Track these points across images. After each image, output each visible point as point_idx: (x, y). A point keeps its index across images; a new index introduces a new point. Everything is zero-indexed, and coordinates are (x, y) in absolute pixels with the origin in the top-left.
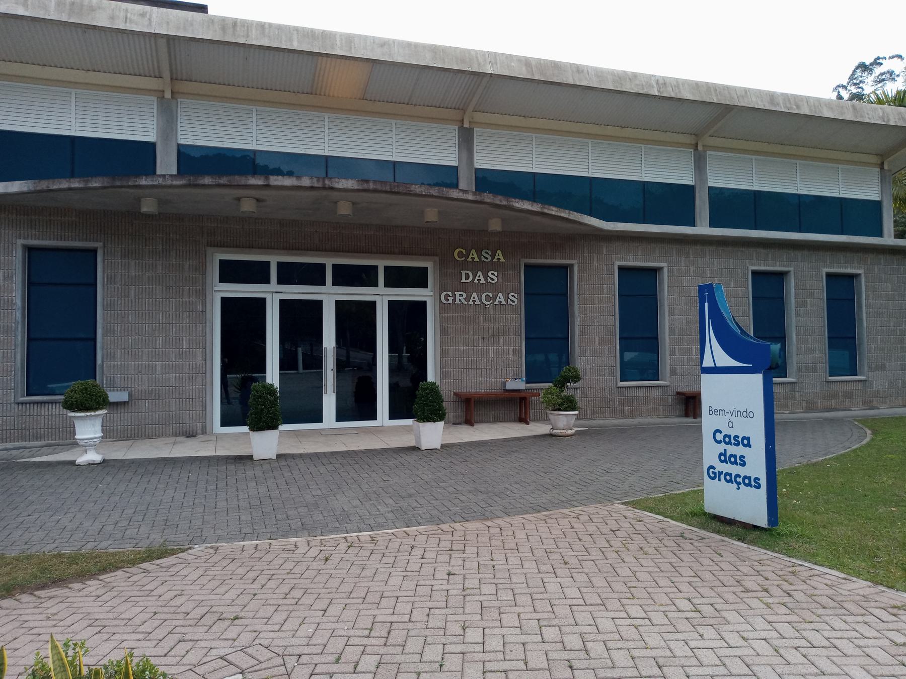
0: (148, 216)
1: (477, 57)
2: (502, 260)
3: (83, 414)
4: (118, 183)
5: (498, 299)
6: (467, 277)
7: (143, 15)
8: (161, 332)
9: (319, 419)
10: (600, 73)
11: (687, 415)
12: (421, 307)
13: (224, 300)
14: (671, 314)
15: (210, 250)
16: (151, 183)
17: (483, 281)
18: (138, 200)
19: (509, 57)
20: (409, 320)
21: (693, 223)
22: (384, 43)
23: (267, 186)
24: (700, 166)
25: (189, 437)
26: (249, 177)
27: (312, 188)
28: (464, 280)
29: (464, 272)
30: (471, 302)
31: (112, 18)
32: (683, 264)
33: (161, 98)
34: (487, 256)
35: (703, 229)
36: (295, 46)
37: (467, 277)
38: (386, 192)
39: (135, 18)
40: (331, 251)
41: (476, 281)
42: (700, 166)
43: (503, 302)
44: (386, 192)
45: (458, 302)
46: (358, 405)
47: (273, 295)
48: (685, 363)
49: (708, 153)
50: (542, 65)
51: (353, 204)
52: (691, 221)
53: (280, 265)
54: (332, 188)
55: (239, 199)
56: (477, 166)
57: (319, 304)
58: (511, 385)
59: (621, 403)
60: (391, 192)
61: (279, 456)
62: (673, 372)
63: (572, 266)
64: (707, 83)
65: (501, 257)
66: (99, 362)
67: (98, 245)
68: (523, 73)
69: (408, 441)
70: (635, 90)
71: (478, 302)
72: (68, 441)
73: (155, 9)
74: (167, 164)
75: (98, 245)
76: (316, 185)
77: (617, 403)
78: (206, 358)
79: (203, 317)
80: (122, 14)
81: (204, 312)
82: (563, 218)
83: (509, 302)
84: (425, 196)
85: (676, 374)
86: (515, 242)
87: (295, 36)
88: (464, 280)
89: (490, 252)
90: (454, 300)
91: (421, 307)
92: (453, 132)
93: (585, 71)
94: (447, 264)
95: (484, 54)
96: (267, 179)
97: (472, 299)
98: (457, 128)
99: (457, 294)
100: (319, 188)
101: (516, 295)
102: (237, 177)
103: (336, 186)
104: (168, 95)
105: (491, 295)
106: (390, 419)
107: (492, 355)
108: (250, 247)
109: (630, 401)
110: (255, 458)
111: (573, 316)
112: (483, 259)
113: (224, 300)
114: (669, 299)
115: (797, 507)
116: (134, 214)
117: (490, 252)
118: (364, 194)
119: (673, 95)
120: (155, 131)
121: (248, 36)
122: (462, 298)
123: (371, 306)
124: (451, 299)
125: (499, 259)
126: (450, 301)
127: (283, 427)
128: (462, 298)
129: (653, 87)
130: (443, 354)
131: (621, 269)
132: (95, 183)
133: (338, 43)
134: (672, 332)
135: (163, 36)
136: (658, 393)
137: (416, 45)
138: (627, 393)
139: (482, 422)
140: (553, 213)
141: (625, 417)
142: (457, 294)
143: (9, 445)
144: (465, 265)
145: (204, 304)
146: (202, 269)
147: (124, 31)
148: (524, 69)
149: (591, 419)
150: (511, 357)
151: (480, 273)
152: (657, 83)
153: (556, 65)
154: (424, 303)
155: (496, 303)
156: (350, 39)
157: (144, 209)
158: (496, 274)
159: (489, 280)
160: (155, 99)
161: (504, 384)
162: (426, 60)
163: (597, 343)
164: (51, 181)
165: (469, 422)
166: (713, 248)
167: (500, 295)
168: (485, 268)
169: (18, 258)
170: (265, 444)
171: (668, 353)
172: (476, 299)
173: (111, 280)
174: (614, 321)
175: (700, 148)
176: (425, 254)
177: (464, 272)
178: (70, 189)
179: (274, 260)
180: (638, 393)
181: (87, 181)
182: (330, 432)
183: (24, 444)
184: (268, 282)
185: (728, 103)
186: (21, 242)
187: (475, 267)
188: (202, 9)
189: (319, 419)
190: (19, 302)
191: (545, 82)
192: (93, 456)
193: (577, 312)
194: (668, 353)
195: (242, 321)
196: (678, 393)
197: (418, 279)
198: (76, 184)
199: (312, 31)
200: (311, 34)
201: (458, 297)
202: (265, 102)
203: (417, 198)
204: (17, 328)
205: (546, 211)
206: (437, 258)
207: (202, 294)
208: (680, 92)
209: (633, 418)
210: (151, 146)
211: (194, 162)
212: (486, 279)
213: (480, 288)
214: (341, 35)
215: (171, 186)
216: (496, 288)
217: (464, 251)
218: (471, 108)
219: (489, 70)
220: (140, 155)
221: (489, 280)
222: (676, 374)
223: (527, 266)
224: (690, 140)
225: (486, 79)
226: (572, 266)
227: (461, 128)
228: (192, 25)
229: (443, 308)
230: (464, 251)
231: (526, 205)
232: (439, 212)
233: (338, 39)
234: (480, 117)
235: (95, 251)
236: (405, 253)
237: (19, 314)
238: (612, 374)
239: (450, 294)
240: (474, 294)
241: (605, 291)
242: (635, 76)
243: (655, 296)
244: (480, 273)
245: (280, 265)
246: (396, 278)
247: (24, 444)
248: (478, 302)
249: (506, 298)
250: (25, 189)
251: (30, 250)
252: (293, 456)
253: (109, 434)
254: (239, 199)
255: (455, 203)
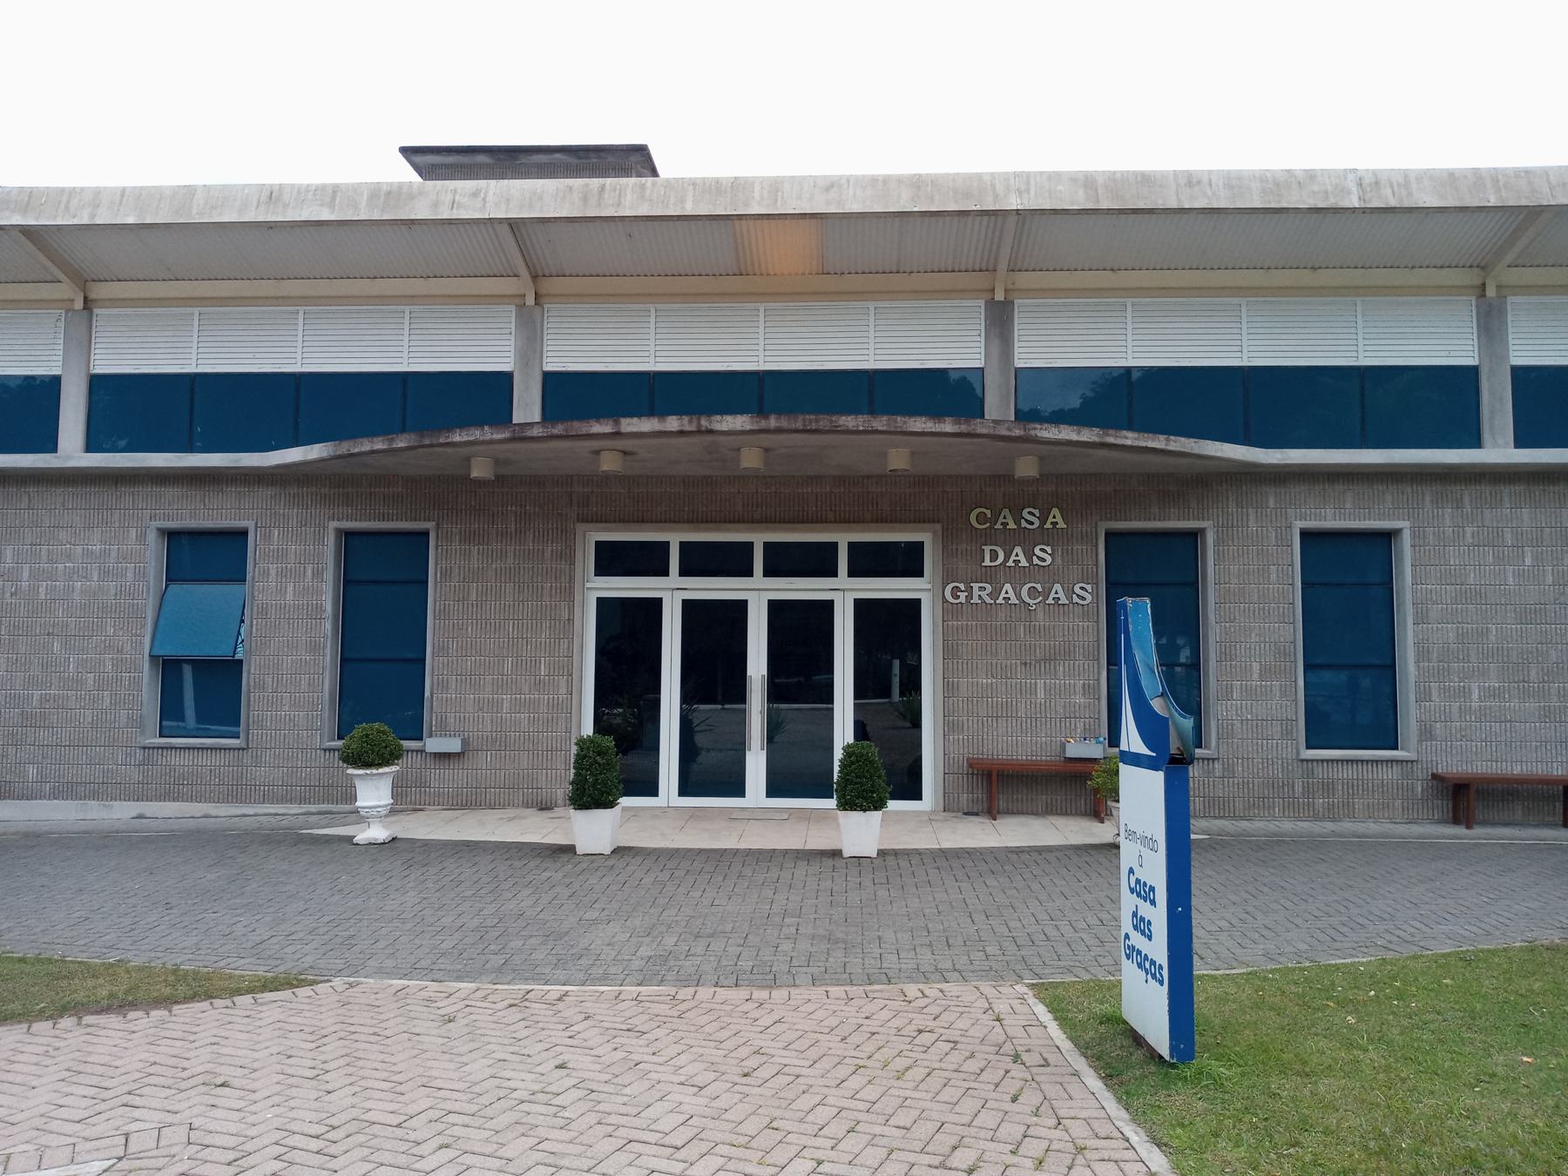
0: (480, 483)
1: (993, 185)
2: (1061, 525)
3: (361, 772)
4: (427, 442)
5: (1052, 595)
6: (994, 556)
7: (475, 195)
8: (514, 656)
9: (740, 792)
10: (1234, 180)
11: (1456, 821)
12: (910, 610)
13: (601, 602)
14: (1421, 618)
15: (580, 527)
16: (466, 438)
17: (1024, 563)
18: (467, 460)
19: (1055, 177)
20: (891, 632)
21: (1477, 443)
22: (831, 185)
23: (617, 434)
24: (1491, 324)
25: (542, 809)
26: (593, 422)
27: (681, 433)
28: (987, 562)
29: (987, 549)
30: (1000, 601)
31: (436, 205)
32: (1448, 522)
33: (521, 306)
34: (1031, 517)
35: (1499, 450)
36: (689, 209)
37: (994, 556)
38: (796, 431)
39: (465, 200)
40: (760, 522)
41: (1010, 563)
42: (1491, 324)
43: (1064, 600)
44: (796, 431)
45: (975, 600)
46: (711, 774)
47: (673, 593)
48: (1456, 716)
49: (1510, 299)
50: (1116, 181)
51: (766, 450)
52: (1474, 439)
53: (684, 546)
54: (711, 432)
55: (597, 452)
56: (1019, 364)
57: (742, 606)
58: (1076, 750)
59: (1308, 790)
60: (805, 431)
61: (618, 851)
62: (1426, 733)
63: (1202, 531)
64: (1476, 171)
65: (1059, 519)
66: (427, 694)
67: (430, 525)
68: (1080, 201)
69: (818, 840)
70: (1309, 203)
71: (1014, 600)
72: (347, 807)
73: (493, 182)
74: (527, 407)
75: (430, 525)
76: (687, 428)
77: (1298, 789)
78: (573, 691)
79: (567, 627)
80: (449, 198)
81: (570, 620)
82: (1154, 450)
83: (1075, 599)
84: (865, 432)
85: (1432, 738)
86: (1075, 491)
87: (690, 194)
88: (987, 562)
89: (1037, 512)
90: (969, 597)
91: (910, 610)
92: (976, 308)
93: (1205, 180)
94: (954, 531)
95: (1006, 177)
96: (617, 423)
97: (1003, 594)
98: (982, 303)
99: (975, 586)
100: (691, 433)
101: (1089, 588)
102: (576, 424)
103: (717, 427)
104: (530, 301)
105: (1039, 587)
106: (920, 798)
107: (1041, 694)
108: (640, 520)
109: (1328, 787)
110: (846, 855)
111: (1206, 624)
112: (1024, 524)
113: (601, 602)
114: (1414, 592)
115: (1351, 1008)
116: (464, 481)
117: (1037, 512)
118: (763, 436)
119: (1393, 203)
120: (512, 354)
121: (619, 204)
122: (983, 594)
123: (738, 610)
124: (963, 596)
125: (1055, 524)
126: (963, 598)
127: (625, 801)
128: (983, 594)
129: (1349, 193)
130: (949, 689)
131: (1306, 535)
132: (401, 442)
133: (757, 195)
134: (1423, 654)
135: (501, 220)
136: (1391, 775)
137: (886, 180)
138: (1319, 771)
139: (1010, 812)
140: (1129, 442)
141: (1316, 818)
142: (975, 586)
143: (313, 808)
144: (990, 537)
145: (571, 610)
146: (568, 556)
147: (450, 222)
148: (1081, 192)
149: (1243, 818)
150: (1079, 699)
151: (1018, 550)
152: (1360, 184)
153: (1145, 179)
154: (916, 604)
155: (1050, 601)
156: (775, 186)
157: (474, 474)
158: (1049, 549)
159: (1036, 561)
160: (513, 308)
161: (1063, 747)
162: (904, 202)
163: (1256, 676)
164: (351, 443)
165: (992, 812)
166: (1520, 488)
167: (1057, 587)
168: (1028, 540)
169: (329, 548)
170: (861, 833)
171: (1412, 698)
172: (1011, 594)
173: (446, 575)
174: (1292, 633)
175: (1491, 292)
176: (920, 520)
177: (987, 549)
178: (373, 452)
179: (675, 539)
180: (1348, 773)
181: (392, 440)
182: (663, 816)
183: (330, 807)
184: (666, 573)
185: (1524, 202)
186: (334, 524)
187: (1009, 540)
188: (633, 160)
189: (740, 792)
190: (329, 608)
191: (1121, 211)
192: (376, 832)
193: (1212, 617)
194: (1412, 698)
195: (627, 638)
196: (1435, 777)
197: (906, 561)
198: (380, 444)
199: (717, 181)
200: (714, 187)
201: (976, 592)
202: (672, 295)
203: (870, 437)
204: (324, 647)
205: (1111, 440)
206: (938, 527)
207: (568, 593)
208: (1410, 194)
209: (1334, 820)
210: (507, 378)
211: (573, 395)
212: (1030, 560)
213: (1018, 576)
214: (763, 180)
215: (492, 442)
216: (1049, 575)
217: (988, 513)
218: (1003, 266)
219: (1014, 203)
220: (490, 393)
221: (1036, 561)
222: (1432, 738)
223: (1109, 535)
224: (1471, 278)
225: (1011, 222)
226: (1202, 531)
227: (991, 304)
228: (541, 198)
229: (949, 611)
230: (988, 513)
231: (1067, 433)
232: (913, 453)
233: (757, 188)
234: (1023, 280)
235: (426, 534)
236: (881, 520)
237: (328, 626)
238: (1288, 734)
239: (962, 586)
240: (1008, 587)
241: (1273, 577)
242: (1311, 175)
243: (1387, 584)
244: (1018, 550)
245: (684, 546)
246: (869, 561)
247: (330, 807)
248: (1014, 600)
249: (1070, 592)
250: (325, 455)
251: (348, 536)
252: (907, 853)
253: (405, 799)
254: (597, 452)
255: (882, 436)
